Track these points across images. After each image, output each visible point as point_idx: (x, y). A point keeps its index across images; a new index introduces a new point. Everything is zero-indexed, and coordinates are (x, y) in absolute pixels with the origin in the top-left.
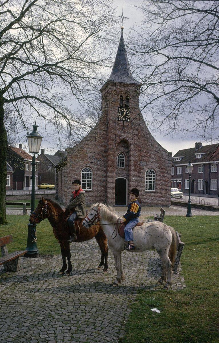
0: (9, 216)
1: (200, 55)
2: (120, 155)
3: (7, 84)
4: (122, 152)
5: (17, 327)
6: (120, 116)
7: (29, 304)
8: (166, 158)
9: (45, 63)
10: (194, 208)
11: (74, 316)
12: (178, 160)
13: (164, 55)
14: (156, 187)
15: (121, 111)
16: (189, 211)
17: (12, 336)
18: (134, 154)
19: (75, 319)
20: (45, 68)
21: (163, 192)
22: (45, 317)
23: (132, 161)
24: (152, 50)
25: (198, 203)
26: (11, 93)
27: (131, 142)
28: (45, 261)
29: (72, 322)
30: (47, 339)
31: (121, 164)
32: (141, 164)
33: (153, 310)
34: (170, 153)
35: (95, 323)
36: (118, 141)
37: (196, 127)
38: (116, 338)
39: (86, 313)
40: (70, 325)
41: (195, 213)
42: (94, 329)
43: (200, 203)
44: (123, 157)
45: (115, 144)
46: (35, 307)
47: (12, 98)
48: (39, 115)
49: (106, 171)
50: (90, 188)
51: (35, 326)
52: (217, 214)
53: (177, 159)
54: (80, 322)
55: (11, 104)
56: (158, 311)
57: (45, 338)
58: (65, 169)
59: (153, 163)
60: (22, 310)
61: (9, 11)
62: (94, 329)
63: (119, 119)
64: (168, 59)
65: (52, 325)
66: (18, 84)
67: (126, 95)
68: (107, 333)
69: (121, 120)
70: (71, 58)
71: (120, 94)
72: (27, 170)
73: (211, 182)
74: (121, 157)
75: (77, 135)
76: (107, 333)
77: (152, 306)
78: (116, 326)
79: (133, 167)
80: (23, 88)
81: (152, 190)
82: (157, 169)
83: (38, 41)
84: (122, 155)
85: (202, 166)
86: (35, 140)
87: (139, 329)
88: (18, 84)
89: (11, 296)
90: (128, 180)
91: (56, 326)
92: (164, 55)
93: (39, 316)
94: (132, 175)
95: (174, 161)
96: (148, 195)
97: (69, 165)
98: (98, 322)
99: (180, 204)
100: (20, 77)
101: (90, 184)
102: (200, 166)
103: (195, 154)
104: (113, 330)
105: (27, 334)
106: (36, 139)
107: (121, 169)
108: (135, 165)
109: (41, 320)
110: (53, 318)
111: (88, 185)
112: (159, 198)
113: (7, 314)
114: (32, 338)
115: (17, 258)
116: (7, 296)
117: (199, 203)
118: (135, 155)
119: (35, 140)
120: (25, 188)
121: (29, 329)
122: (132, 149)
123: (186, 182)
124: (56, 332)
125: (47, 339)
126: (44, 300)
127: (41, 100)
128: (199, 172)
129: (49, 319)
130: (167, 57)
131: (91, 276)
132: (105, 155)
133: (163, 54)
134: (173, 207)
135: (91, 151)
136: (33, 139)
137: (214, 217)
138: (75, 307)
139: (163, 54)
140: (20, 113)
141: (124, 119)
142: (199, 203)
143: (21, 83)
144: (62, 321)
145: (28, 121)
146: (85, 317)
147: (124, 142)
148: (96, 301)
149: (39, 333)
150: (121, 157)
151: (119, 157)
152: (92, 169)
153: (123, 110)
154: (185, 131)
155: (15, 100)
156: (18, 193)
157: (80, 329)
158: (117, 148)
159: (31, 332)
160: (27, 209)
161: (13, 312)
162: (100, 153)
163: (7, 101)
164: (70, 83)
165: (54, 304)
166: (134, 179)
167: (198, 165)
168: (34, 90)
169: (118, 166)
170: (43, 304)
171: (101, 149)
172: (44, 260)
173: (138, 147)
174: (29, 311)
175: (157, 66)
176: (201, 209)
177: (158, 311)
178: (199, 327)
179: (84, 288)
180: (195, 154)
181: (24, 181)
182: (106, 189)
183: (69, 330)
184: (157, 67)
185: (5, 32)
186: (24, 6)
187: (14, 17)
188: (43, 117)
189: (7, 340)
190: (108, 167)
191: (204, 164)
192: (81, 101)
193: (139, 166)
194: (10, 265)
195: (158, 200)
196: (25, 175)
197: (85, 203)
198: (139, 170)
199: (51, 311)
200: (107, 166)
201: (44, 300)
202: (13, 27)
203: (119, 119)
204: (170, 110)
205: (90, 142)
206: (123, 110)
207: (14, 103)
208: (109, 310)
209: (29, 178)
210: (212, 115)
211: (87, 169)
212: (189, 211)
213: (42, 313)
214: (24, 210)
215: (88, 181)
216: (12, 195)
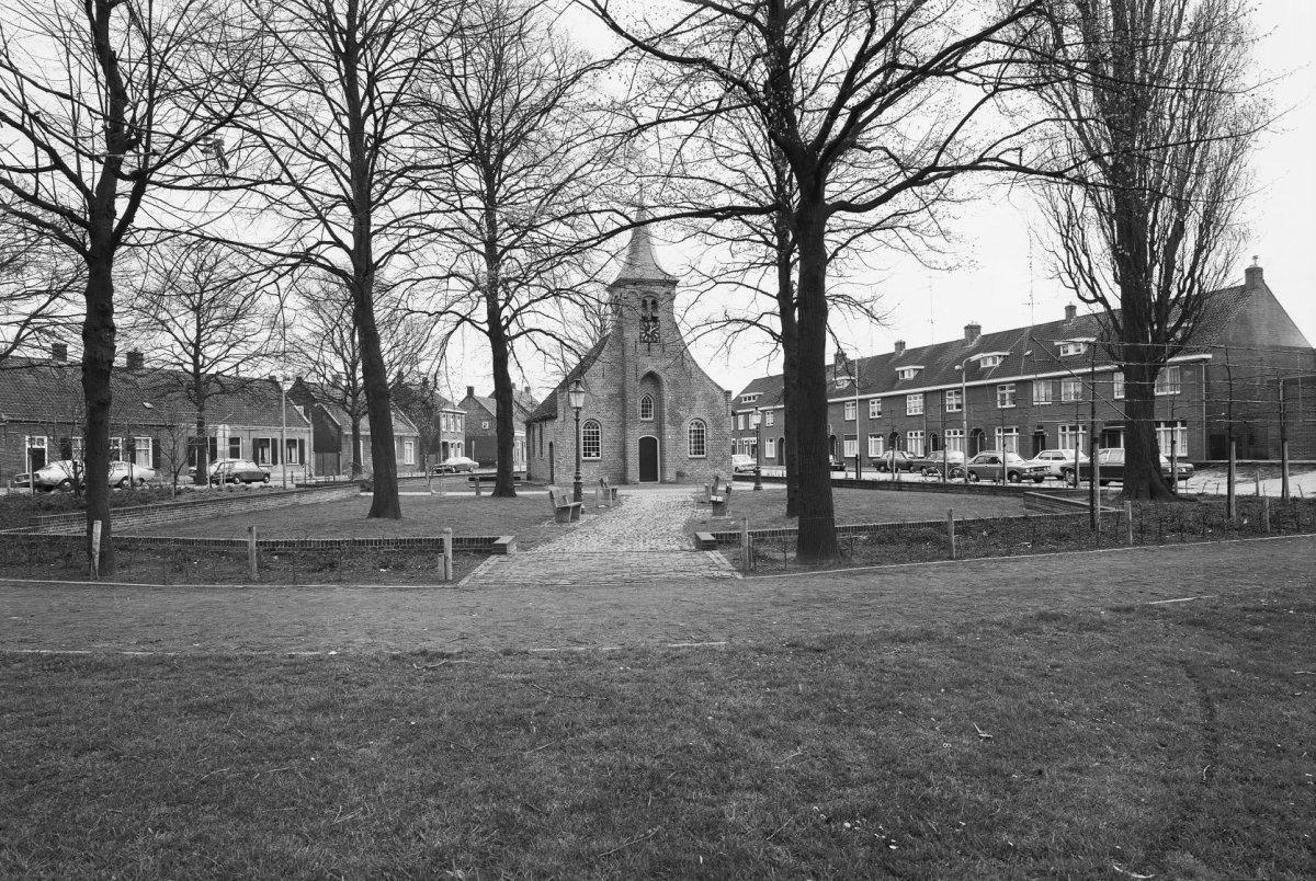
8: (721, 400)
9: (483, 211)
12: (752, 401)
21: (719, 458)
27: (664, 377)
34: (728, 393)
36: (641, 375)
41: (765, 486)
49: (624, 426)
53: (750, 398)
59: (700, 411)
67: (651, 299)
69: (645, 342)
73: (946, 435)
81: (701, 456)
85: (1011, 388)
90: (660, 438)
96: (694, 463)
102: (1003, 388)
107: (647, 422)
108: (670, 414)
122: (666, 388)
128: (999, 407)
147: (652, 377)
162: (611, 397)
164: (581, 306)
167: (844, 402)
169: (643, 416)
171: (614, 390)
173: (675, 384)
182: (623, 455)
191: (925, 393)
197: (231, 678)
198: (677, 422)
216: (412, 478)
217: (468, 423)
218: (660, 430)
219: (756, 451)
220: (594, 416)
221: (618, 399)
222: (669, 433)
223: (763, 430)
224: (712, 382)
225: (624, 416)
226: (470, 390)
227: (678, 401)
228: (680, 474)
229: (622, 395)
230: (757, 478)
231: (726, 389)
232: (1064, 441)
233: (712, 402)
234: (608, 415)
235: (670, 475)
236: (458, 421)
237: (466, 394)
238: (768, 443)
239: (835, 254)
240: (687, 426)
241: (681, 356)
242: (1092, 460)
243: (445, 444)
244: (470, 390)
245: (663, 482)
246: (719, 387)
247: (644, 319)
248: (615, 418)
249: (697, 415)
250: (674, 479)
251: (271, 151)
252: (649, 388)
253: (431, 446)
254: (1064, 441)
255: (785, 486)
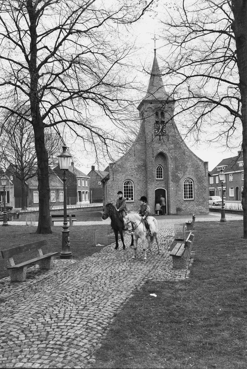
0: (36, 221)
1: (220, 71)
2: (158, 167)
3: (47, 110)
4: (160, 165)
5: (38, 307)
6: (157, 131)
7: (52, 292)
10: (227, 213)
11: (84, 300)
13: (183, 74)
14: (194, 195)
15: (157, 126)
16: (223, 216)
17: (32, 313)
18: (171, 166)
19: (84, 301)
20: (79, 94)
21: (201, 200)
22: (62, 300)
23: (170, 173)
24: (171, 71)
25: (237, 209)
26: (51, 118)
27: (169, 155)
28: (76, 261)
29: (82, 303)
30: (58, 314)
31: (159, 175)
32: (179, 175)
33: (151, 295)
34: (206, 164)
35: (99, 304)
36: (155, 154)
37: (219, 137)
38: (111, 314)
39: (95, 297)
40: (79, 305)
42: (97, 307)
43: (240, 209)
44: (162, 169)
45: (153, 157)
46: (56, 294)
47: (53, 122)
48: (78, 136)
49: (146, 182)
50: (132, 199)
51: (52, 306)
52: (241, 218)
54: (88, 303)
55: (52, 127)
56: (155, 296)
57: (57, 314)
58: (109, 182)
59: (190, 174)
60: (45, 296)
61: (46, 47)
62: (97, 307)
63: (156, 134)
64: (185, 78)
65: (65, 306)
66: (57, 110)
68: (106, 310)
69: (157, 135)
70: (72, 94)
71: (157, 111)
72: (79, 185)
74: (159, 169)
75: (122, 150)
76: (106, 310)
77: (152, 292)
78: (116, 306)
79: (171, 178)
80: (62, 114)
81: (191, 199)
82: (194, 179)
83: (64, 75)
84: (160, 167)
86: (64, 159)
87: (134, 308)
88: (57, 110)
89: (40, 287)
90: (167, 191)
91: (68, 306)
92: (183, 74)
93: (57, 299)
94: (171, 185)
95: (218, 170)
96: (187, 203)
97: (111, 179)
98: (102, 303)
99: (219, 211)
100: (58, 104)
101: (132, 196)
103: (238, 162)
104: (112, 309)
105: (43, 312)
106: (66, 158)
107: (160, 180)
108: (172, 176)
109: (58, 302)
110: (68, 301)
111: (130, 196)
112: (197, 205)
113: (33, 299)
114: (47, 314)
115: (49, 258)
116: (37, 287)
117: (238, 209)
118: (172, 166)
119: (64, 159)
120: (78, 203)
121: (46, 308)
122: (170, 161)
123: (230, 190)
124: (66, 310)
125: (58, 314)
126: (65, 289)
127: (78, 122)
129: (64, 301)
130: (185, 76)
131: (110, 272)
132: (144, 167)
133: (181, 74)
134: (212, 214)
135: (132, 164)
136: (63, 158)
137: (239, 221)
138: (88, 293)
139: (181, 74)
140: (61, 135)
141: (160, 133)
142: (238, 209)
143: (60, 109)
144: (74, 303)
145: (68, 142)
146: (93, 300)
147: (162, 155)
148: (107, 289)
149: (53, 311)
150: (159, 169)
151: (157, 169)
152: (133, 182)
153: (159, 125)
154: (209, 142)
155: (56, 123)
156: (73, 207)
157: (86, 308)
158: (155, 161)
159: (47, 310)
160: (73, 221)
161: (37, 298)
162: (139, 167)
163: (47, 126)
165: (71, 291)
166: (172, 189)
167: (229, 174)
168: (70, 115)
170: (63, 292)
172: (75, 261)
173: (175, 159)
174: (50, 297)
175: (177, 85)
176: (238, 214)
177: (155, 296)
178: (184, 306)
179: (100, 280)
180: (238, 162)
181: (76, 196)
183: (77, 309)
184: (177, 86)
185: (44, 64)
186: (56, 42)
187: (50, 52)
188: (81, 137)
189: (28, 315)
190: (148, 179)
192: (114, 121)
193: (177, 176)
194: (44, 264)
195: (196, 208)
196: (78, 190)
199: (68, 296)
200: (146, 178)
201: (65, 289)
202: (49, 60)
203: (156, 134)
204: (193, 123)
205: (130, 157)
206: (159, 125)
207: (55, 126)
208: (115, 295)
209: (82, 193)
210: (233, 126)
211: (128, 182)
212: (223, 216)
213: (60, 298)
214: (65, 221)
215: (130, 193)
217: (91, 183)
218: (167, 186)
219: (224, 193)
220: (130, 177)
221: (143, 168)
222: (172, 187)
223: (228, 183)
224: (196, 157)
225: (146, 177)
226: (93, 168)
227: (177, 168)
228: (178, 210)
229: (145, 165)
230: (223, 212)
231: (205, 161)
232: (85, 198)
233: (197, 168)
234: (138, 177)
235: (173, 210)
236: (87, 182)
237: (91, 170)
238: (230, 190)
239: (29, 110)
240: (182, 183)
241: (179, 143)
242: (156, 205)
243: (80, 192)
244: (93, 168)
245: (169, 214)
246: (201, 160)
247: (157, 122)
248: (141, 178)
249: (188, 176)
250: (175, 212)
251: (185, 12)
252: (160, 161)
253: (72, 194)
254: (85, 198)
255: (241, 218)
